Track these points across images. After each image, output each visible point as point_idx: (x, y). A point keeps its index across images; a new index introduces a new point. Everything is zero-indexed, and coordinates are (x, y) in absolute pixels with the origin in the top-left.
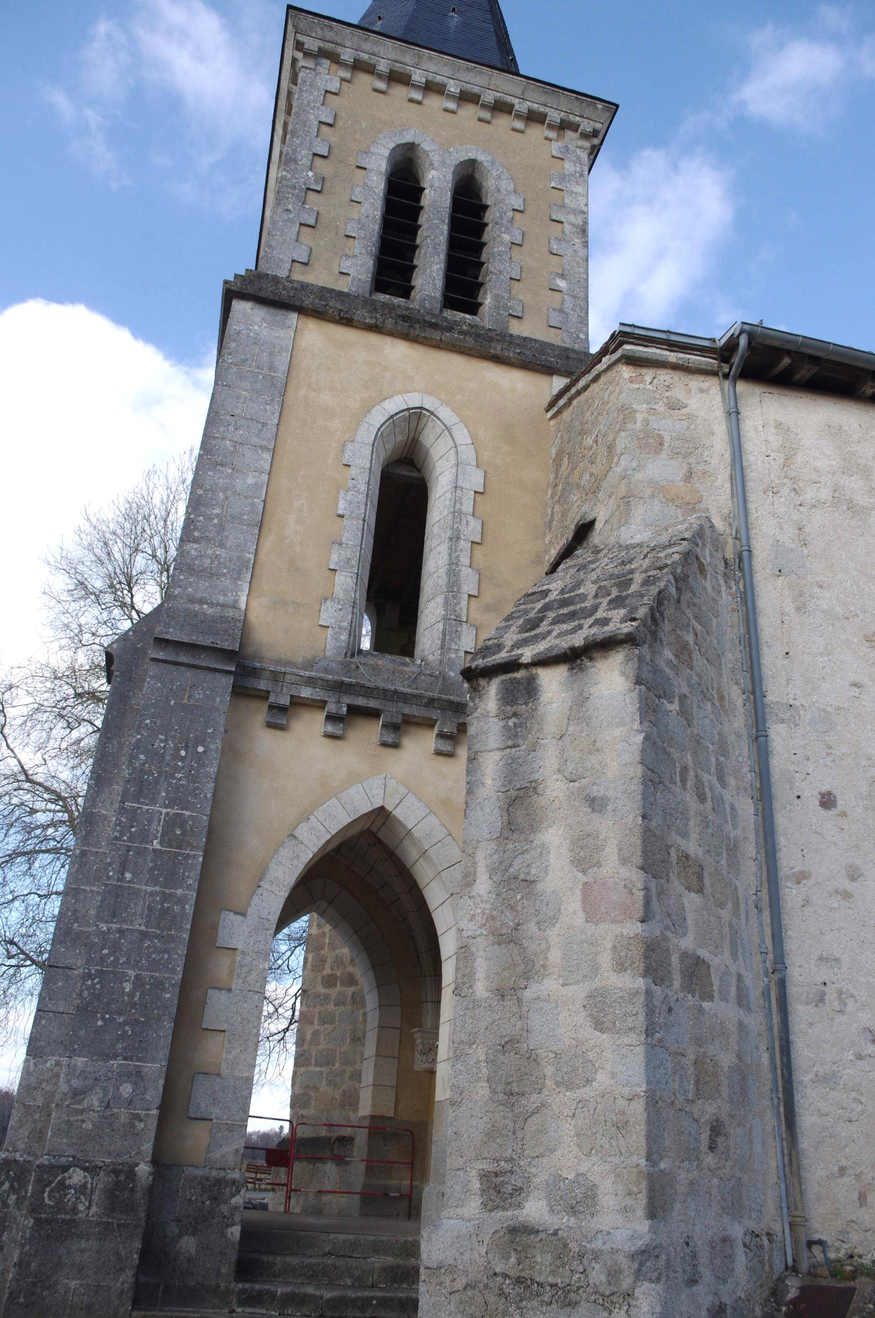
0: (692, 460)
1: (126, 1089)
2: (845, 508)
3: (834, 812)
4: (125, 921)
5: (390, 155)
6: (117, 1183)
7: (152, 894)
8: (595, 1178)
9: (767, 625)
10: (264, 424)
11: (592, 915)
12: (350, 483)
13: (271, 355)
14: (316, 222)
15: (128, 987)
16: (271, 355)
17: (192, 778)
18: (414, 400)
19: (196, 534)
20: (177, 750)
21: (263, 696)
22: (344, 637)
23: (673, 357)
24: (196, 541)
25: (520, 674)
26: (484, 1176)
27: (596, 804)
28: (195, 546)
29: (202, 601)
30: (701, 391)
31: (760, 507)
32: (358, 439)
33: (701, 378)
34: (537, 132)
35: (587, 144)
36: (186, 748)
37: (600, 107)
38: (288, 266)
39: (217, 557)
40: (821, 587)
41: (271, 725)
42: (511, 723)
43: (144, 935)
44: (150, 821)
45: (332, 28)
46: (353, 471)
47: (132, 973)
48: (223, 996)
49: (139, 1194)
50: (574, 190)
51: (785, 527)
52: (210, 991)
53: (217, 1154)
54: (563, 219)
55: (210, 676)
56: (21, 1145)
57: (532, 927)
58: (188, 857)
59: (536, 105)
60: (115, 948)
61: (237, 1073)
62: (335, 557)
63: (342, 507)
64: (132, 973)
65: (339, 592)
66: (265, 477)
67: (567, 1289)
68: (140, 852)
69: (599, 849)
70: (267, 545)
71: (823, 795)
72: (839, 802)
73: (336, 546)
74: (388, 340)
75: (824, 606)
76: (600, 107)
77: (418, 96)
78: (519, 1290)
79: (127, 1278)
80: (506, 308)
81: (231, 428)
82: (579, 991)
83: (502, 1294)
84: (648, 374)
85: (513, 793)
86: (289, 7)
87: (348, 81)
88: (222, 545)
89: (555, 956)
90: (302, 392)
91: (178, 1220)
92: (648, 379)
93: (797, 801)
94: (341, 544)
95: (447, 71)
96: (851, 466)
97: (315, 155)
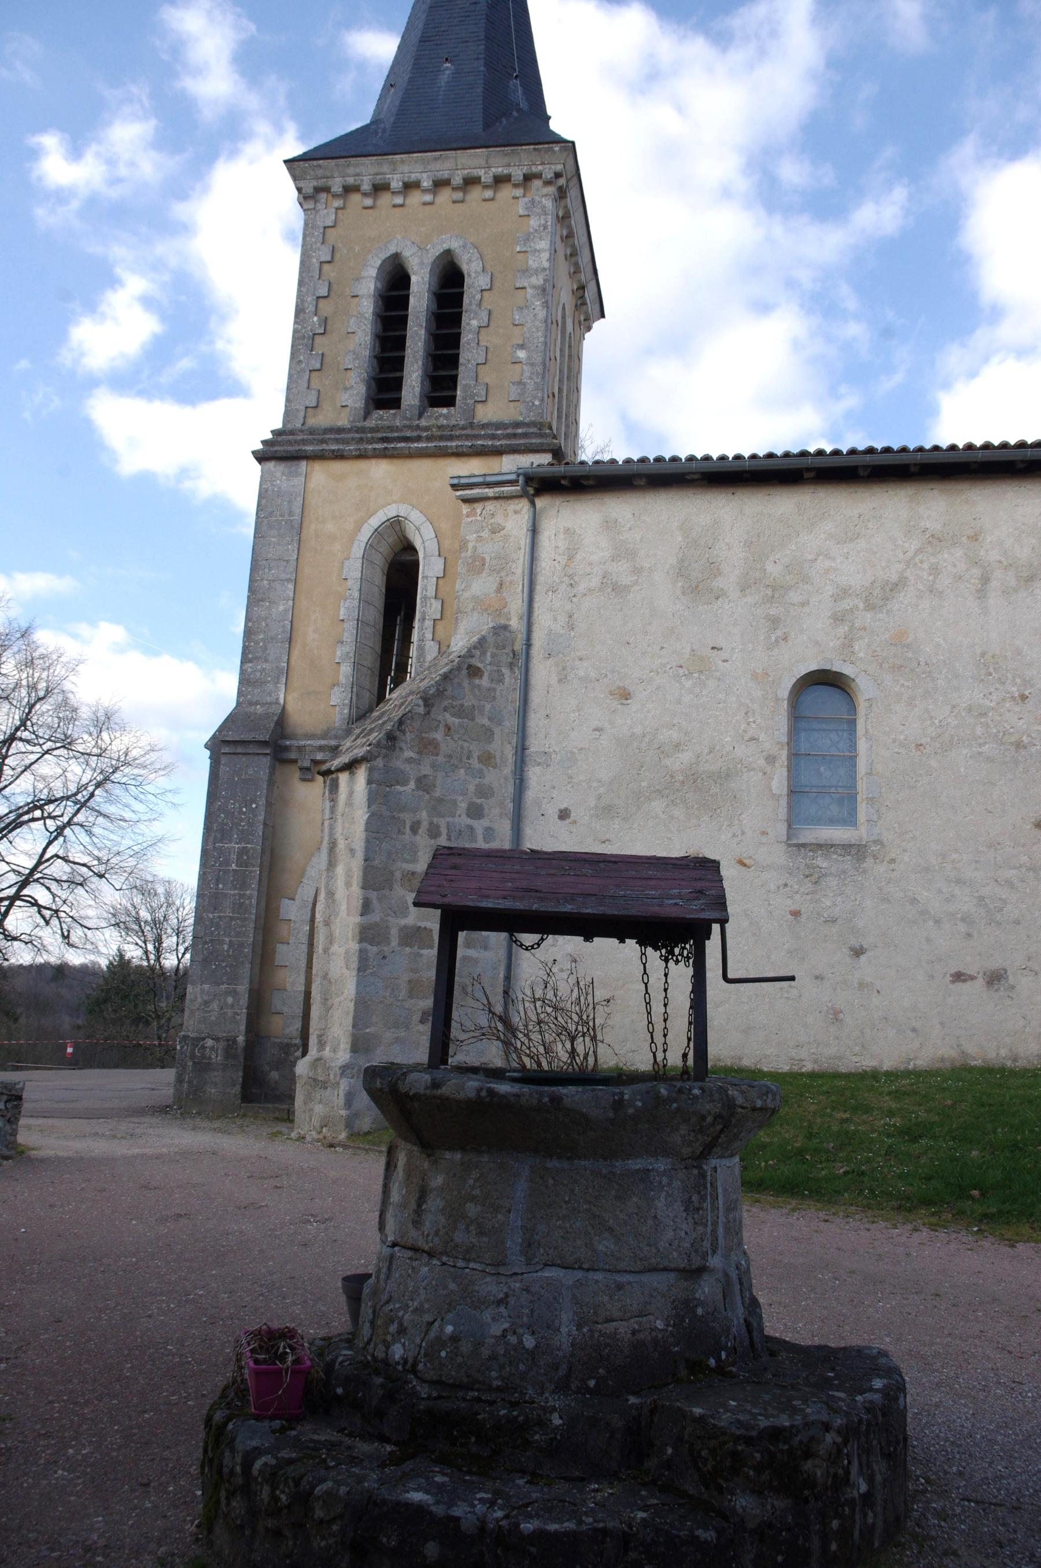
0: (503, 574)
1: (230, 1000)
2: (610, 590)
3: (568, 821)
4: (221, 911)
5: (378, 273)
6: (229, 1046)
7: (234, 895)
9: (536, 697)
10: (288, 561)
12: (348, 593)
13: (290, 502)
14: (322, 364)
15: (226, 947)
16: (290, 502)
17: (250, 824)
18: (391, 511)
19: (250, 656)
20: (241, 808)
21: (294, 761)
22: (346, 711)
23: (490, 492)
24: (250, 661)
28: (250, 665)
29: (257, 703)
30: (516, 512)
32: (352, 556)
33: (517, 501)
34: (506, 192)
35: (551, 190)
36: (246, 806)
37: (557, 149)
38: (302, 414)
39: (264, 670)
40: (581, 659)
41: (304, 780)
43: (232, 918)
44: (229, 853)
45: (320, 166)
46: (350, 583)
47: (227, 939)
48: (285, 946)
49: (239, 1051)
50: (538, 248)
51: (559, 618)
52: (278, 945)
53: (287, 1031)
54: (526, 285)
55: (256, 758)
56: (191, 1028)
58: (251, 872)
59: (500, 169)
60: (218, 927)
61: (295, 988)
62: (339, 653)
63: (342, 614)
64: (227, 939)
65: (342, 679)
66: (291, 603)
68: (226, 872)
70: (295, 653)
71: (561, 811)
72: (573, 814)
73: (339, 645)
74: (374, 461)
75: (581, 673)
76: (557, 149)
77: (399, 200)
79: (237, 1089)
80: (473, 396)
81: (267, 570)
84: (478, 507)
86: (285, 162)
87: (343, 208)
88: (266, 661)
90: (313, 527)
91: (268, 1063)
92: (479, 511)
93: (542, 818)
94: (342, 643)
95: (419, 167)
96: (623, 552)
97: (318, 298)
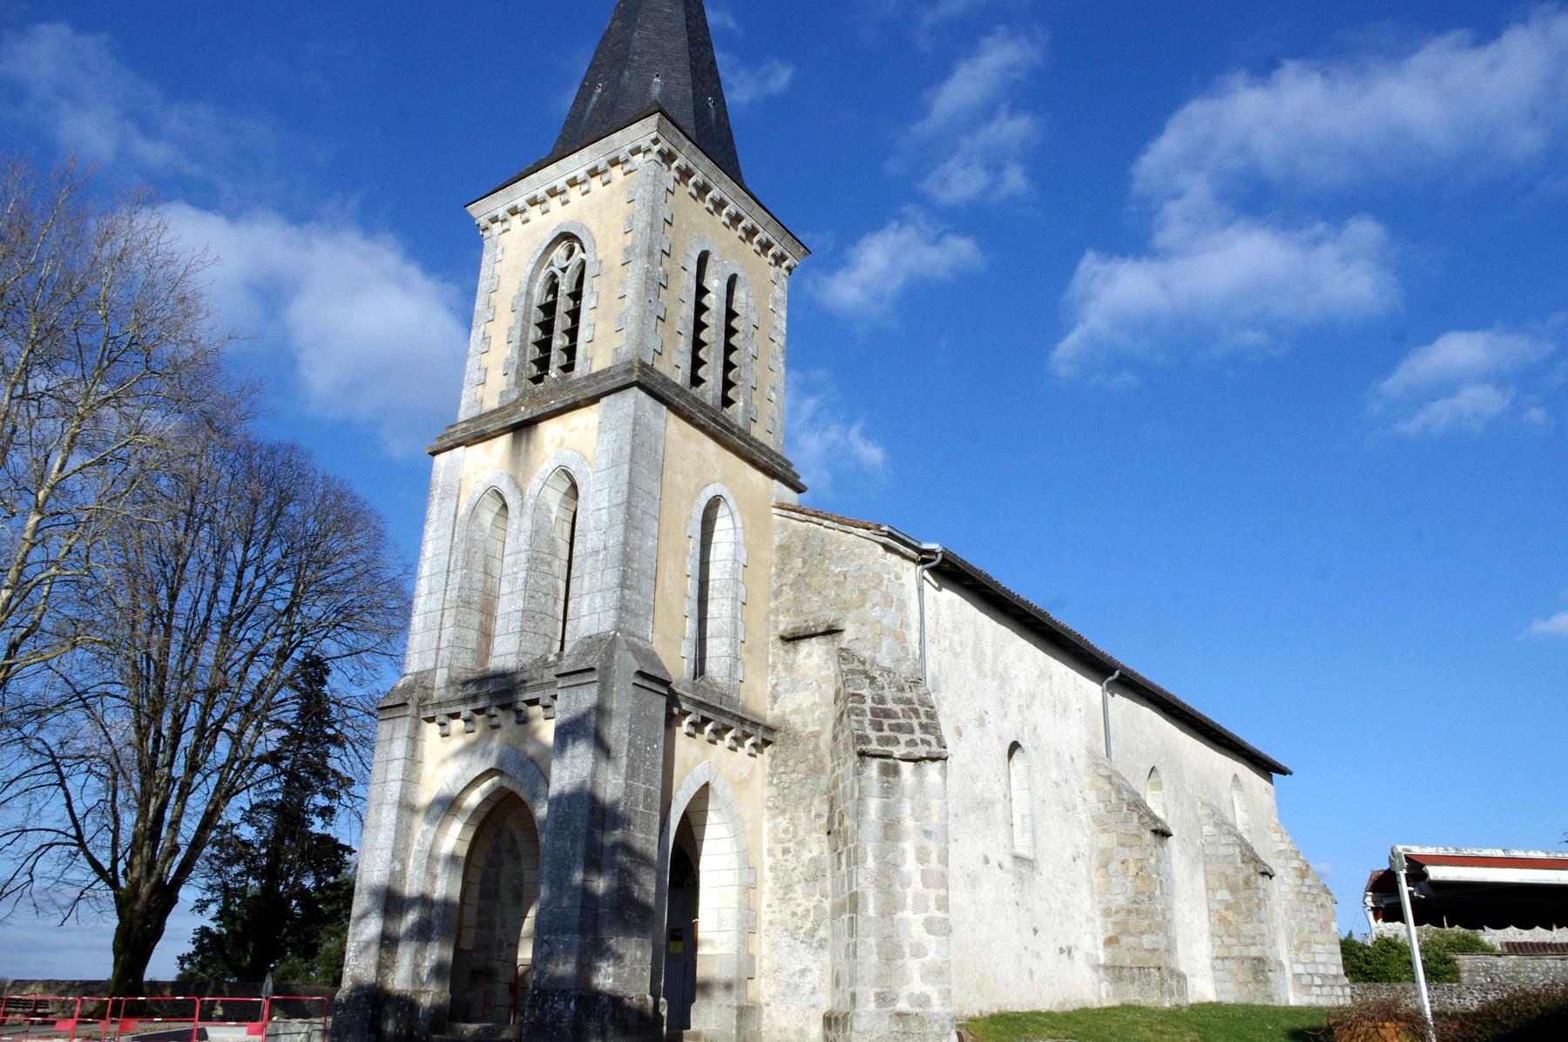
11: (925, 883)
23: (902, 548)
25: (890, 761)
31: (931, 651)
82: (921, 917)
89: (909, 901)
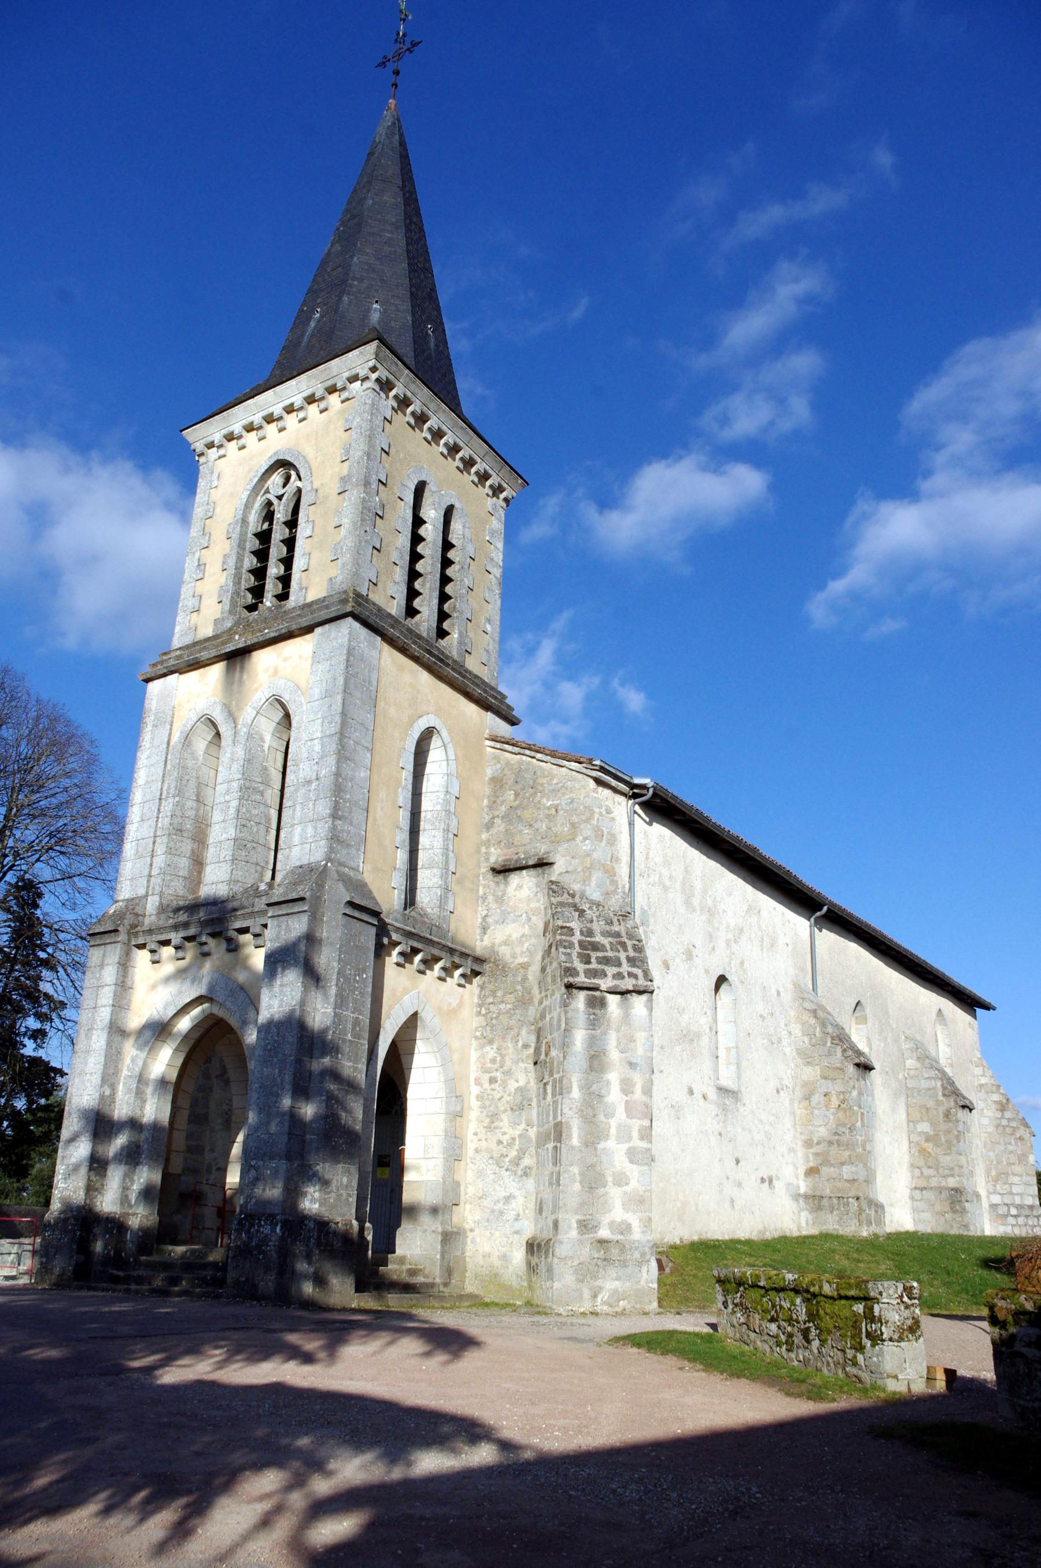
8: (630, 1221)
23: (614, 783)
25: (597, 994)
26: (579, 1222)
27: (632, 1065)
42: (592, 1017)
57: (602, 1118)
67: (625, 1261)
69: (634, 1086)
78: (605, 1263)
82: (624, 1147)
83: (597, 1265)
85: (593, 1053)
88: (351, 824)
89: (613, 1131)
